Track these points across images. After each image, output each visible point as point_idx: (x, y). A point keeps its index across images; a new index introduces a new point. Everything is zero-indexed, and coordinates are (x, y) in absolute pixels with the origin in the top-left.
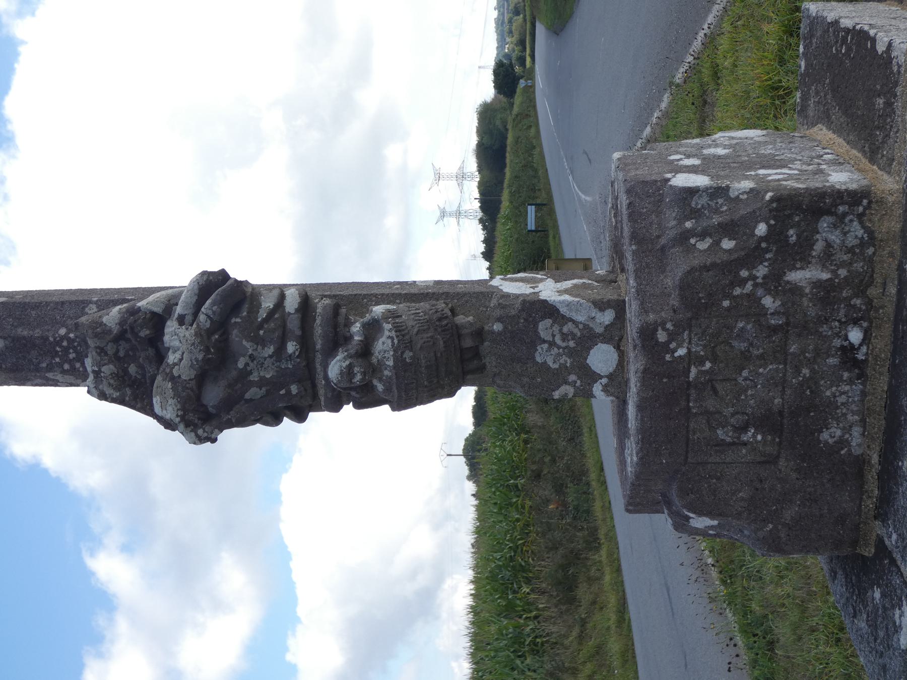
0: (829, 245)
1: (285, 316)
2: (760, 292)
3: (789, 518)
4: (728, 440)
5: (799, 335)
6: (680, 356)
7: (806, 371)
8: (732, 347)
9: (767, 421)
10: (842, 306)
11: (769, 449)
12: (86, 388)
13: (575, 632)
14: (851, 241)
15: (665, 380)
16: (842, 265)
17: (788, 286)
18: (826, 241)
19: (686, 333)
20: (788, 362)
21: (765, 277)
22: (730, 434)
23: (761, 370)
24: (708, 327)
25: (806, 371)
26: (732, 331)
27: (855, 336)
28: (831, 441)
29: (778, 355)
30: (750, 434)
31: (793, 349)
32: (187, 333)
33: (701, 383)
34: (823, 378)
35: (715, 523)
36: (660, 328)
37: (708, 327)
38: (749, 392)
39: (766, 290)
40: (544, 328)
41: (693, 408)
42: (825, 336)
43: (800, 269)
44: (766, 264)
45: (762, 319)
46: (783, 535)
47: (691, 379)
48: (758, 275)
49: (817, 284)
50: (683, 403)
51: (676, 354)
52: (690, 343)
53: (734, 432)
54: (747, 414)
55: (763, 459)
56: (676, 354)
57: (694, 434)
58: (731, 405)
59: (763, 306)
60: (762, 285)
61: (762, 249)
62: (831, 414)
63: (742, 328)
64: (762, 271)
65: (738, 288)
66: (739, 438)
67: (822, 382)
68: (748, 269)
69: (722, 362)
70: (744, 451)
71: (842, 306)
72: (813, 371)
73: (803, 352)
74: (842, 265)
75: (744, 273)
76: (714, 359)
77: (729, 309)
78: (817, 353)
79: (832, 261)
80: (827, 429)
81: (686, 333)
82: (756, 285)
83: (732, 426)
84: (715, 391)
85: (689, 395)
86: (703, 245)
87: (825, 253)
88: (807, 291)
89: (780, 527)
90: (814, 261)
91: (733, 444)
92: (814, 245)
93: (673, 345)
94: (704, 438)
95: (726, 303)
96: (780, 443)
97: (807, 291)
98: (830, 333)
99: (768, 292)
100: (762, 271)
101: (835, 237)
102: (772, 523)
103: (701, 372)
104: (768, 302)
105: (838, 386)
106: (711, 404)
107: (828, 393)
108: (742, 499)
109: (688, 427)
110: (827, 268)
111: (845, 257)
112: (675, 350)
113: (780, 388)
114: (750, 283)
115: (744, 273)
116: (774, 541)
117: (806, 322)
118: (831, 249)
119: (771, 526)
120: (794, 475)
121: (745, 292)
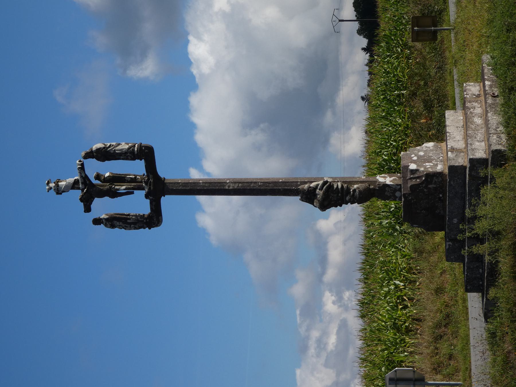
1: (338, 189)
12: (300, 197)
14: (439, 180)
27: (441, 196)
31: (430, 197)
32: (321, 192)
40: (387, 189)
49: (434, 187)
64: (424, 185)
86: (414, 180)
100: (424, 185)
101: (436, 180)
104: (425, 190)
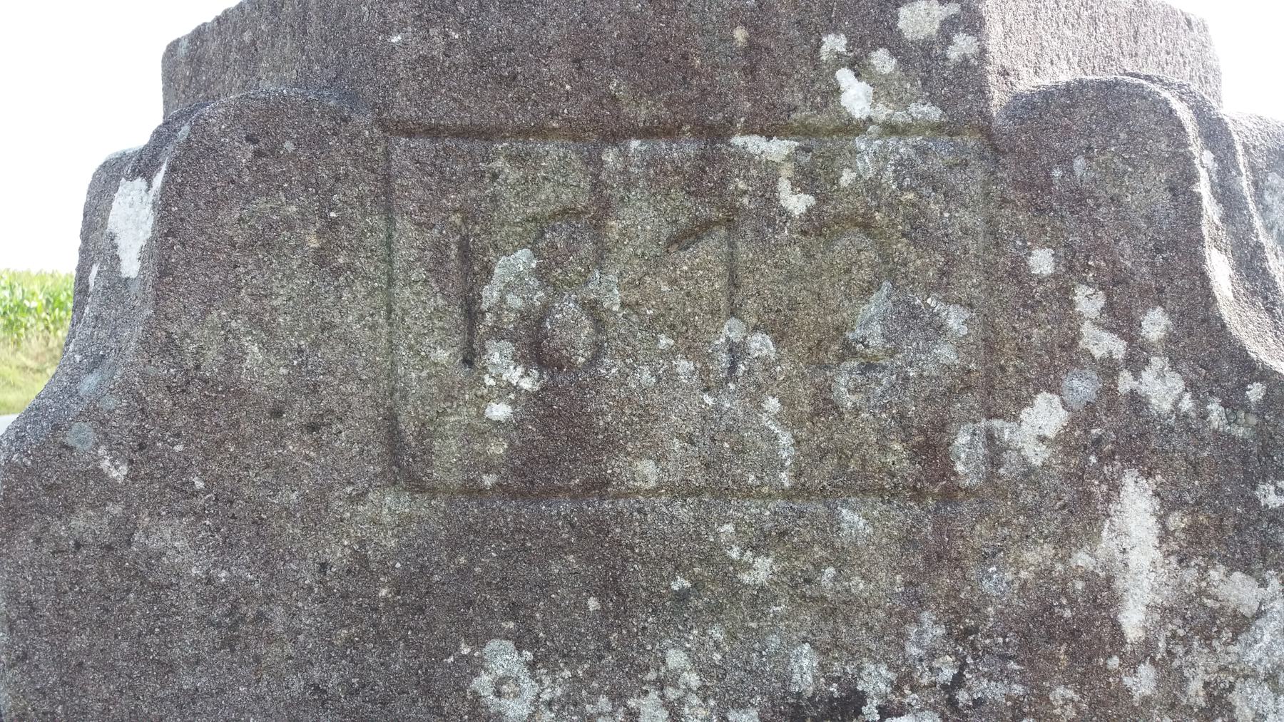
0: (1241, 624)
2: (1083, 387)
3: (154, 544)
4: (490, 295)
5: (908, 541)
6: (837, 91)
7: (762, 570)
8: (866, 292)
9: (566, 437)
10: (1018, 689)
11: (449, 450)
13: (31, 363)
15: (740, 34)
16: (1172, 678)
17: (1099, 489)
18: (1260, 614)
19: (934, 113)
20: (798, 504)
21: (1137, 402)
22: (515, 301)
23: (772, 404)
24: (950, 195)
25: (762, 570)
26: (930, 289)
28: (483, 683)
29: (830, 464)
30: (514, 375)
31: (853, 520)
33: (723, 182)
34: (732, 636)
35: (130, 267)
36: (954, 9)
37: (950, 195)
38: (684, 366)
39: (1090, 407)
41: (624, 154)
42: (902, 635)
43: (1164, 527)
44: (1187, 404)
45: (972, 399)
46: (78, 523)
47: (738, 140)
48: (1148, 376)
49: (1103, 594)
50: (642, 114)
51: (845, 77)
52: (891, 129)
53: (524, 316)
54: (594, 361)
55: (408, 428)
56: (845, 77)
57: (517, 159)
58: (635, 296)
59: (1023, 402)
60: (1109, 391)
61: (1243, 387)
62: (592, 675)
63: (940, 329)
64: (1162, 389)
65: (1100, 301)
66: (498, 333)
67: (717, 633)
68: (1170, 339)
69: (809, 255)
70: (442, 355)
71: (1018, 689)
72: (760, 598)
73: (842, 558)
74: (1172, 678)
75: (1155, 324)
76: (817, 226)
77: (1018, 272)
78: (834, 610)
79: (1185, 641)
80: (532, 666)
81: (934, 113)
82: (1108, 369)
83: (547, 309)
84: (685, 238)
85: (670, 132)
87: (1213, 614)
88: (1082, 559)
89: (116, 509)
90: (1190, 575)
91: (472, 313)
92: (1248, 572)
93: (883, 61)
94: (494, 198)
95: (1042, 262)
96: (473, 491)
97: (1082, 559)
98: (913, 651)
99: (1083, 418)
100: (1162, 389)
102: (133, 478)
103: (770, 173)
104: (1044, 417)
105: (704, 693)
106: (639, 220)
107: (675, 659)
108: (233, 357)
109: (542, 132)
110: (1162, 624)
111: (1195, 686)
112: (859, 67)
113: (698, 479)
114: (1118, 348)
115: (1155, 324)
116: (50, 488)
117: (957, 562)
118: (1227, 635)
119: (119, 473)
120: (338, 554)
121: (1087, 329)
